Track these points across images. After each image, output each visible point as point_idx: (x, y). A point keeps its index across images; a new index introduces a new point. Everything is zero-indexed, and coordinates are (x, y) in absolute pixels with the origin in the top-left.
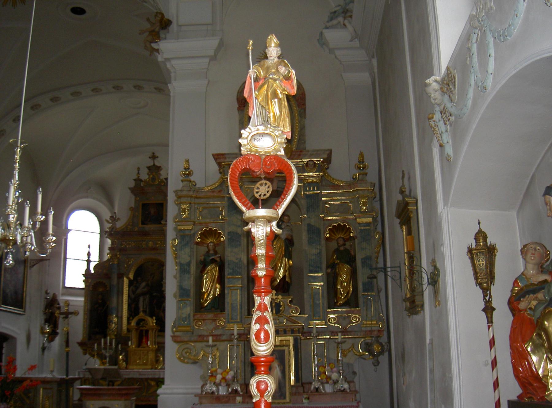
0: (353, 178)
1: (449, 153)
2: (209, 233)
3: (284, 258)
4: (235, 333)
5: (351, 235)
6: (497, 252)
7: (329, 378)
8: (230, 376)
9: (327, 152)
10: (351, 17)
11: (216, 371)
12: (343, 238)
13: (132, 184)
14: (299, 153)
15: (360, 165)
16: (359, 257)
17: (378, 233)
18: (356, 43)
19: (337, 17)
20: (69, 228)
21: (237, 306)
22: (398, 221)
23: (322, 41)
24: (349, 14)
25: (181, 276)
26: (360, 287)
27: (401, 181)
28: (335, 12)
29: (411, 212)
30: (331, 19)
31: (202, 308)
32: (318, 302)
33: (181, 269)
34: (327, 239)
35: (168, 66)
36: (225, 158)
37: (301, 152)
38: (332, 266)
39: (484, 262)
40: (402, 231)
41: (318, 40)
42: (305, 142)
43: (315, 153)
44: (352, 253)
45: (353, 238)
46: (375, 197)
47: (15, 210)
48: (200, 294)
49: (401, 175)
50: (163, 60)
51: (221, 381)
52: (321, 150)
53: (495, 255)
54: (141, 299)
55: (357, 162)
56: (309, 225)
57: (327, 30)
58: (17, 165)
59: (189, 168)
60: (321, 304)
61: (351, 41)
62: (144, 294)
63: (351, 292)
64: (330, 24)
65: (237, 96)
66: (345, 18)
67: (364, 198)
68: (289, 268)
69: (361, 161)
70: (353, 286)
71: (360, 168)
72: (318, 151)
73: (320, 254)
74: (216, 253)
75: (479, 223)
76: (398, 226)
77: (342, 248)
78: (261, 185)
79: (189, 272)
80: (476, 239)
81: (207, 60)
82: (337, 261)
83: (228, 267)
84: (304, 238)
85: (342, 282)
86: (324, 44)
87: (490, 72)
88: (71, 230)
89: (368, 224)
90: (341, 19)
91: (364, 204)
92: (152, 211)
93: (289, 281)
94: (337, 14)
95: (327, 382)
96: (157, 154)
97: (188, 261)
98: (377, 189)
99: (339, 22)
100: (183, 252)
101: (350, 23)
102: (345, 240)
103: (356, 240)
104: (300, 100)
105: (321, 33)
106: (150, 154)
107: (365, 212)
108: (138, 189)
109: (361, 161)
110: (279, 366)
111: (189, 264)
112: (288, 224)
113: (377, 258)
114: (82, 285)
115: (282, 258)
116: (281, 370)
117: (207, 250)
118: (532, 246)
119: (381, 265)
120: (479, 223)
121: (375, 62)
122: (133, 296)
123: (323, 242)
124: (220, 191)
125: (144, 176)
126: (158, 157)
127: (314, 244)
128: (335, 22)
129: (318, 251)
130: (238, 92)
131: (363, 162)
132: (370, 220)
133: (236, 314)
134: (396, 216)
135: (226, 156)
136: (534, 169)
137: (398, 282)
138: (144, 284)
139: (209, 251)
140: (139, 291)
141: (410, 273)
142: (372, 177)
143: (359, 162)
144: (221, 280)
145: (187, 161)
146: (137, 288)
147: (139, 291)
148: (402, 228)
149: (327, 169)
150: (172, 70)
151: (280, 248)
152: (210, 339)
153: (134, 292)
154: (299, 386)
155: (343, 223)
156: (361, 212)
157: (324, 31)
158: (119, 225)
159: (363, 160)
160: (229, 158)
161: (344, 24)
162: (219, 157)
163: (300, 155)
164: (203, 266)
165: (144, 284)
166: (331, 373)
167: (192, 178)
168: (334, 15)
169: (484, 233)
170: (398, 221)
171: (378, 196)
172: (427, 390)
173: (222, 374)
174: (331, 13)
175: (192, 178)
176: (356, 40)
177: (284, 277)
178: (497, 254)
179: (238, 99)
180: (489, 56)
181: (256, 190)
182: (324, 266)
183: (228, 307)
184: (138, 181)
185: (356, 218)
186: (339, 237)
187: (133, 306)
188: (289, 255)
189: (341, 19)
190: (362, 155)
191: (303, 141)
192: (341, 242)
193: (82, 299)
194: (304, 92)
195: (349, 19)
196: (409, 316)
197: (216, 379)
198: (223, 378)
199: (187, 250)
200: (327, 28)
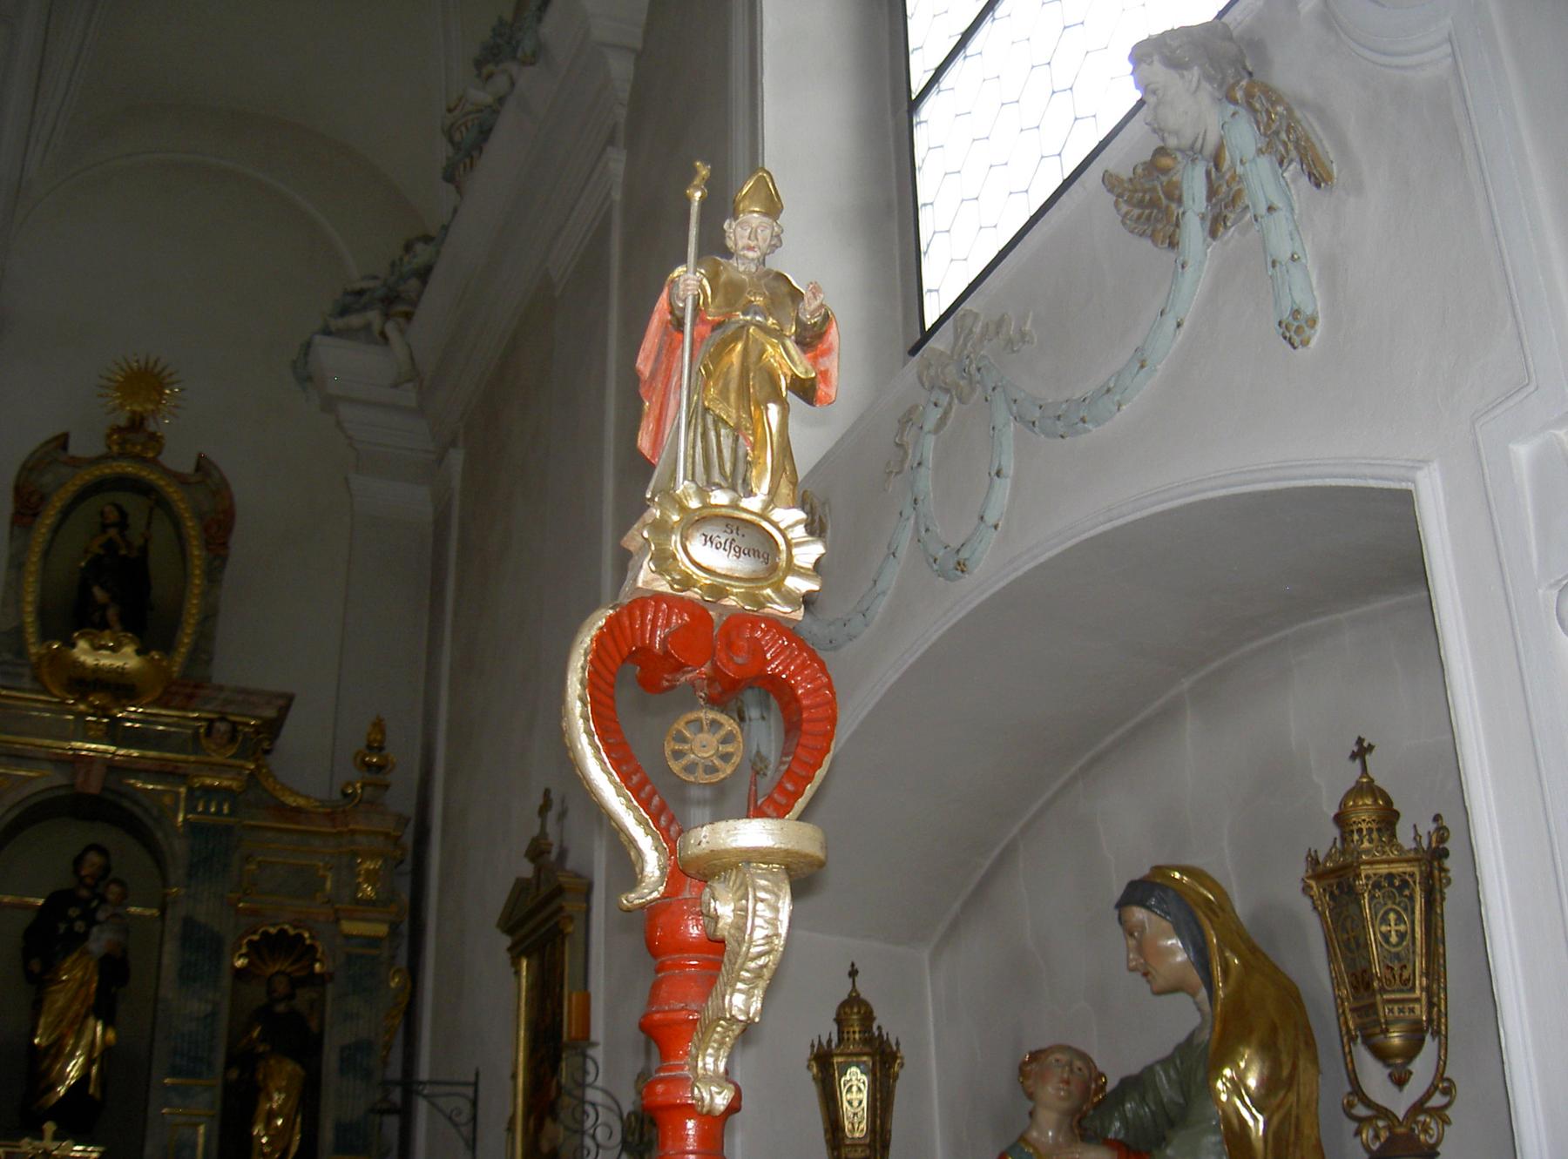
0: (345, 795)
1: (764, 751)
3: (91, 1021)
5: (317, 966)
6: (902, 1065)
9: (281, 702)
10: (408, 316)
12: (288, 975)
15: (371, 756)
16: (335, 1039)
17: (398, 971)
19: (365, 308)
22: (507, 941)
23: (304, 373)
24: (402, 308)
26: (327, 1135)
27: (538, 821)
28: (360, 293)
29: (571, 918)
30: (344, 311)
34: (239, 973)
37: (196, 686)
38: (244, 1061)
39: (864, 1096)
40: (518, 973)
41: (294, 362)
42: (211, 659)
44: (314, 1025)
45: (323, 979)
46: (402, 862)
49: (539, 801)
53: (896, 1077)
55: (362, 745)
56: (189, 923)
57: (328, 340)
61: (395, 386)
63: (294, 1149)
64: (341, 323)
66: (387, 316)
67: (372, 856)
68: (102, 1054)
69: (376, 747)
70: (302, 1131)
71: (369, 766)
75: (853, 973)
76: (504, 957)
77: (281, 1008)
78: (698, 725)
80: (840, 1021)
82: (261, 1048)
84: (166, 960)
85: (271, 1115)
87: (991, 518)
89: (373, 941)
90: (374, 316)
91: (371, 877)
93: (98, 1096)
94: (365, 299)
98: (408, 839)
99: (368, 327)
101: (402, 332)
102: (295, 983)
103: (330, 986)
105: (308, 346)
107: (369, 902)
109: (376, 747)
113: (388, 1047)
118: (1059, 1056)
119: (395, 1071)
120: (853, 973)
121: (457, 457)
123: (226, 981)
126: (1360, 741)
128: (355, 320)
129: (209, 1008)
131: (381, 749)
132: (381, 930)
134: (499, 925)
136: (1015, 830)
137: (466, 1130)
141: (530, 1109)
142: (401, 799)
143: (370, 747)
148: (515, 963)
149: (267, 752)
151: (81, 985)
155: (295, 927)
156: (358, 902)
157: (318, 339)
159: (382, 742)
161: (383, 334)
163: (190, 697)
168: (353, 301)
169: (866, 1004)
170: (507, 941)
171: (409, 858)
174: (346, 293)
176: (410, 386)
177: (84, 1079)
178: (902, 1074)
179: (18, 490)
180: (998, 474)
181: (670, 746)
182: (220, 1058)
185: (337, 920)
186: (277, 973)
188: (105, 1009)
189: (374, 316)
190: (379, 725)
192: (281, 986)
195: (401, 320)
200: (327, 332)
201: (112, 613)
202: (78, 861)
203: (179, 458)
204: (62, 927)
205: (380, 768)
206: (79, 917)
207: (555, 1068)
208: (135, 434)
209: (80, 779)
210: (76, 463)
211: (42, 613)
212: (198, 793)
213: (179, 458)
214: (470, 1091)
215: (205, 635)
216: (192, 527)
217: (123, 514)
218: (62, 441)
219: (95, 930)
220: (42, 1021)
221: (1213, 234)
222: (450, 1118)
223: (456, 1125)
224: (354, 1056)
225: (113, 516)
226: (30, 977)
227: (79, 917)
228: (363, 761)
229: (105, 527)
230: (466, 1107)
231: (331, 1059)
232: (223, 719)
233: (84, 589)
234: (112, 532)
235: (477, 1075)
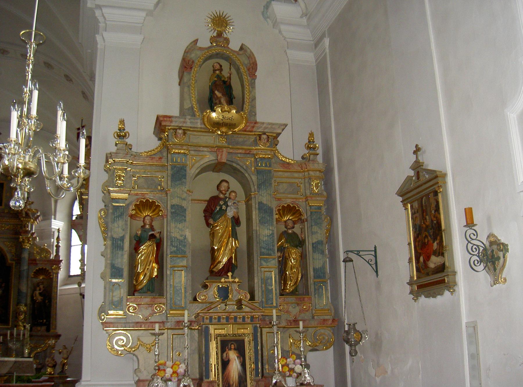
2: (145, 205)
4: (186, 321)
7: (292, 370)
8: (182, 369)
9: (283, 127)
11: (165, 364)
14: (252, 125)
18: (305, 20)
21: (181, 289)
22: (401, 199)
25: (112, 253)
26: (311, 273)
31: (135, 291)
32: (270, 288)
33: (113, 244)
35: (98, 13)
36: (171, 122)
40: (406, 209)
43: (270, 126)
48: (133, 275)
50: (94, 6)
51: (171, 375)
52: (277, 124)
56: (260, 203)
58: (31, 66)
59: (124, 129)
60: (274, 290)
65: (184, 55)
71: (311, 148)
72: (273, 124)
73: (273, 234)
74: (152, 228)
79: (122, 248)
81: (144, 14)
83: (172, 244)
84: (254, 217)
86: (268, 17)
95: (290, 376)
97: (121, 235)
100: (116, 225)
104: (251, 69)
110: (238, 357)
111: (122, 239)
112: (235, 201)
115: (229, 238)
116: (240, 362)
117: (143, 224)
121: (327, 41)
124: (160, 158)
126: (417, 146)
127: (266, 225)
129: (271, 232)
130: (185, 52)
133: (179, 299)
135: (173, 119)
137: (374, 266)
139: (145, 225)
143: (309, 142)
144: (159, 260)
145: (122, 122)
150: (101, 19)
152: (157, 326)
154: (259, 380)
155: (293, 204)
160: (176, 122)
162: (165, 119)
164: (137, 243)
166: (294, 366)
167: (129, 141)
170: (401, 199)
173: (172, 368)
175: (129, 141)
179: (184, 59)
183: (169, 291)
191: (253, 114)
192: (290, 224)
194: (255, 61)
196: (415, 301)
197: (166, 373)
198: (174, 372)
199: (121, 223)
201: (223, 100)
202: (218, 187)
203: (235, 46)
204: (218, 208)
205: (314, 148)
206: (224, 204)
207: (214, 254)
208: (219, 38)
209: (219, 157)
210: (201, 49)
211: (199, 102)
212: (258, 160)
213: (235, 46)
214: (373, 253)
215: (253, 107)
216: (243, 69)
217: (221, 66)
218: (196, 41)
219: (229, 208)
220: (55, 254)
221: (45, 63)
222: (368, 262)
223: (370, 265)
224: (316, 246)
225: (218, 67)
226: (208, 224)
227: (224, 204)
228: (308, 146)
229: (214, 71)
230: (373, 258)
231: (309, 247)
232: (264, 134)
233: (212, 92)
234: (217, 72)
235: (375, 247)
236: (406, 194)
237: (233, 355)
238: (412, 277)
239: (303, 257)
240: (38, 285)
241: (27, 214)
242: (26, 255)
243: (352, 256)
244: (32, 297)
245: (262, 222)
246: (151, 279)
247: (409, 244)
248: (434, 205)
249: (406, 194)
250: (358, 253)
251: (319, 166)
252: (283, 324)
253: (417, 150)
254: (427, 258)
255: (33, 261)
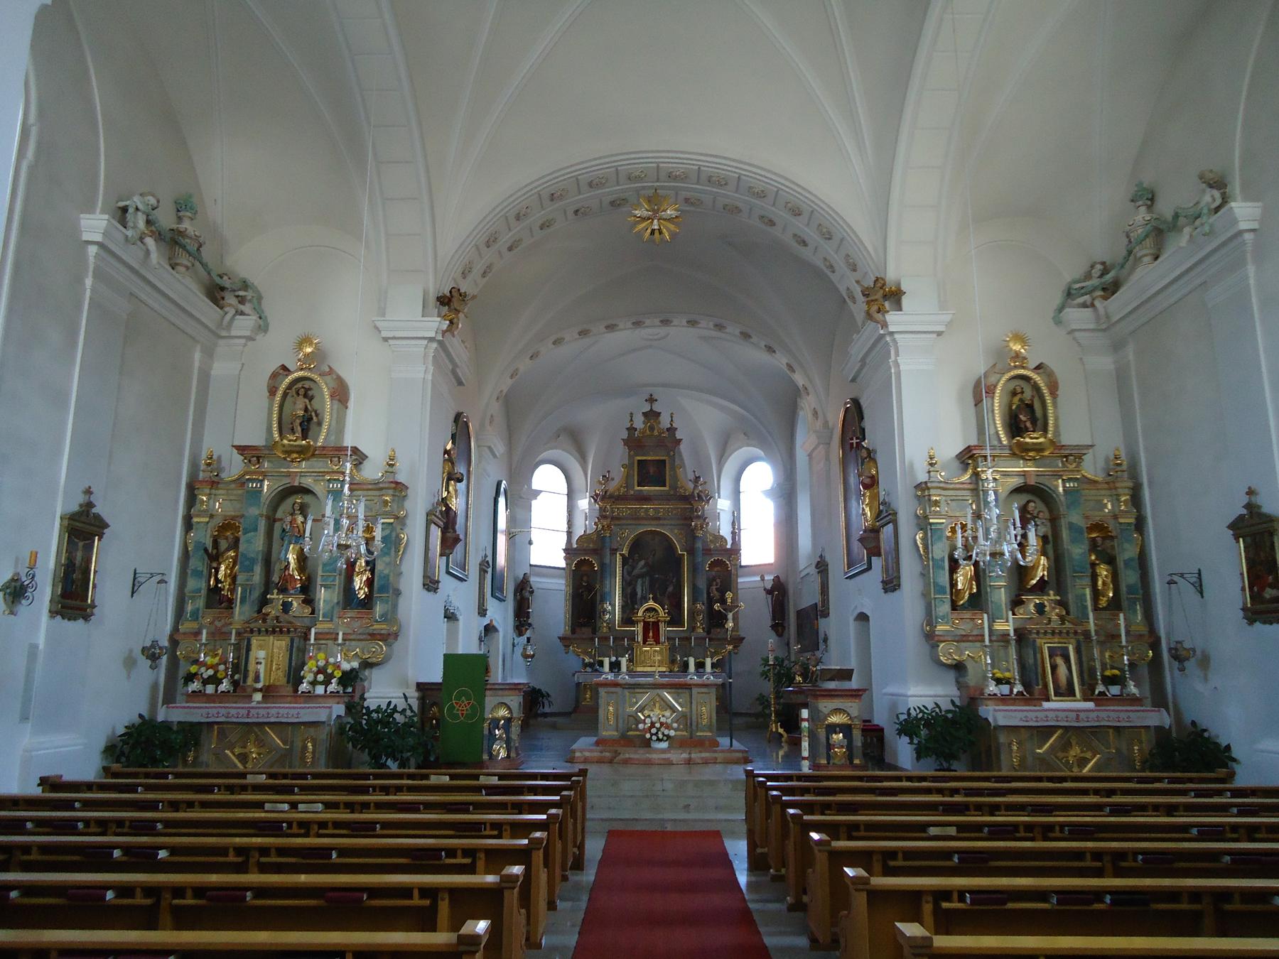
13: (625, 435)
20: (535, 486)
47: (1030, 632)
54: (640, 581)
62: (641, 576)
88: (538, 493)
92: (652, 470)
96: (655, 397)
106: (647, 397)
108: (634, 442)
114: (563, 564)
122: (628, 578)
125: (639, 422)
138: (642, 563)
140: (636, 572)
146: (634, 568)
147: (636, 572)
153: (629, 573)
158: (612, 487)
165: (642, 563)
172: (104, 195)
184: (631, 429)
187: (629, 591)
193: (563, 582)
231: (1121, 564)
236: (1238, 527)
237: (1059, 661)
238: (1245, 603)
239: (1115, 576)
240: (714, 579)
241: (699, 496)
242: (699, 545)
243: (1175, 578)
244: (708, 594)
245: (1074, 541)
246: (971, 595)
247: (1242, 574)
248: (1268, 544)
249: (1238, 527)
250: (1182, 575)
251: (1126, 478)
252: (1102, 639)
253: (1251, 492)
254: (1262, 589)
255: (707, 552)
